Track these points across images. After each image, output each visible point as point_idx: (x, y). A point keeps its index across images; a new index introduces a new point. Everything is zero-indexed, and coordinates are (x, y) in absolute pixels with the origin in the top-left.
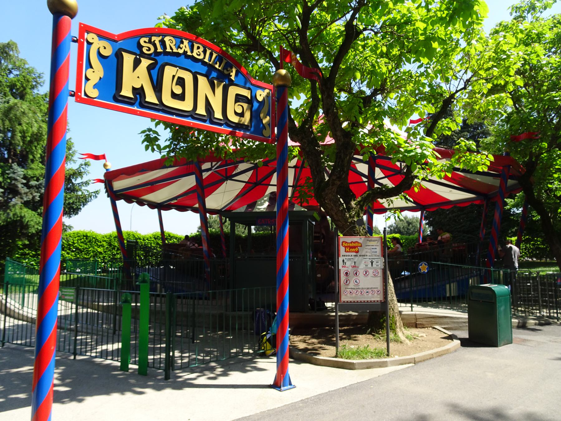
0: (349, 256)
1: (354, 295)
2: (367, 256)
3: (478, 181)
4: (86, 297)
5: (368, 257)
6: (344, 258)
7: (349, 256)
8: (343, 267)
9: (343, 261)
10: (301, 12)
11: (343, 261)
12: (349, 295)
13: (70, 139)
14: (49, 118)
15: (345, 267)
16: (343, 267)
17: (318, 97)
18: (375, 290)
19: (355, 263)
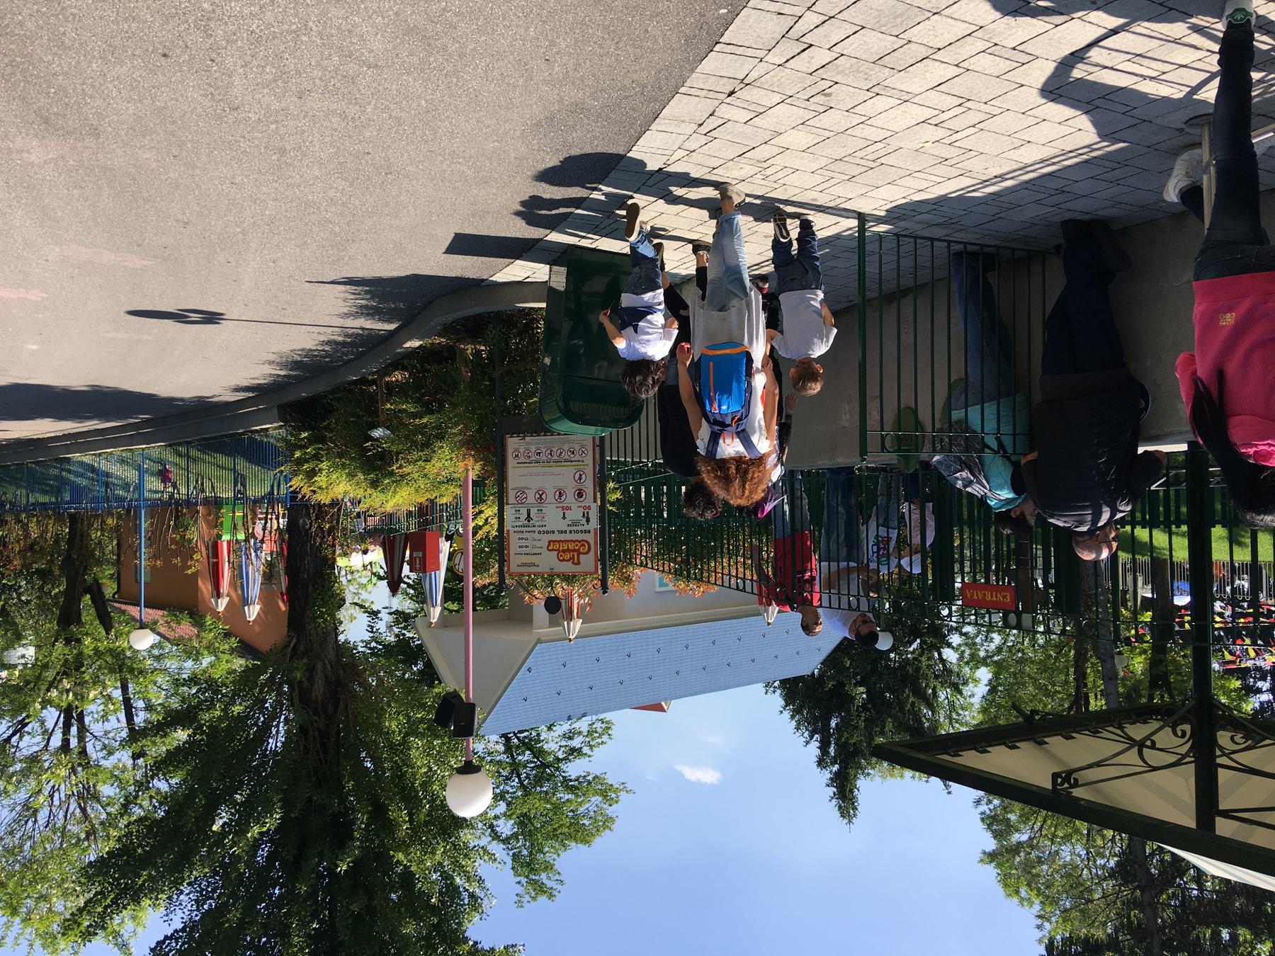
0: (577, 532)
1: (566, 447)
2: (539, 532)
3: (305, 398)
4: (907, 339)
5: (537, 529)
6: (586, 527)
7: (577, 532)
8: (589, 508)
9: (588, 521)
10: (1076, 792)
11: (588, 521)
12: (577, 447)
13: (807, 743)
14: (1249, 84)
15: (585, 508)
16: (589, 508)
17: (953, 542)
18: (522, 460)
19: (564, 517)
